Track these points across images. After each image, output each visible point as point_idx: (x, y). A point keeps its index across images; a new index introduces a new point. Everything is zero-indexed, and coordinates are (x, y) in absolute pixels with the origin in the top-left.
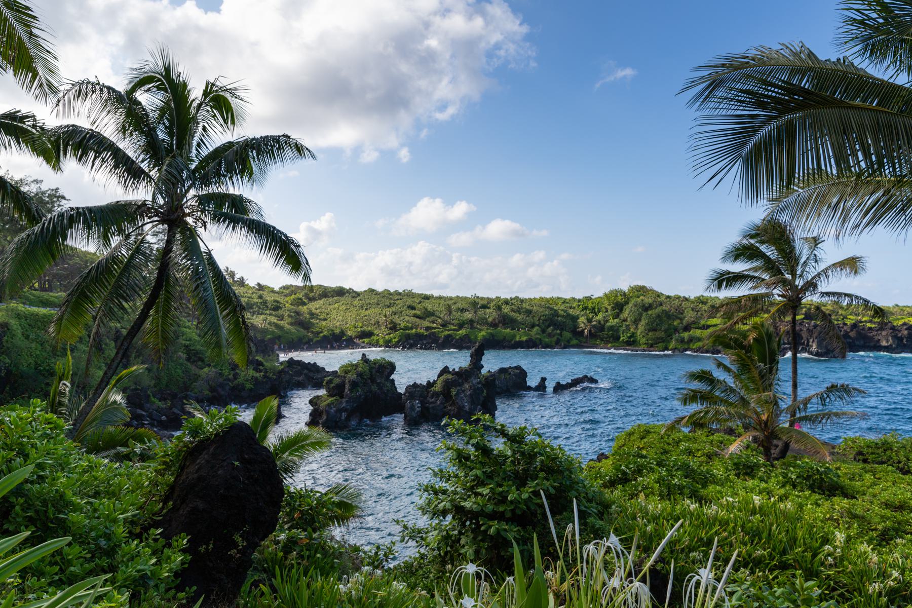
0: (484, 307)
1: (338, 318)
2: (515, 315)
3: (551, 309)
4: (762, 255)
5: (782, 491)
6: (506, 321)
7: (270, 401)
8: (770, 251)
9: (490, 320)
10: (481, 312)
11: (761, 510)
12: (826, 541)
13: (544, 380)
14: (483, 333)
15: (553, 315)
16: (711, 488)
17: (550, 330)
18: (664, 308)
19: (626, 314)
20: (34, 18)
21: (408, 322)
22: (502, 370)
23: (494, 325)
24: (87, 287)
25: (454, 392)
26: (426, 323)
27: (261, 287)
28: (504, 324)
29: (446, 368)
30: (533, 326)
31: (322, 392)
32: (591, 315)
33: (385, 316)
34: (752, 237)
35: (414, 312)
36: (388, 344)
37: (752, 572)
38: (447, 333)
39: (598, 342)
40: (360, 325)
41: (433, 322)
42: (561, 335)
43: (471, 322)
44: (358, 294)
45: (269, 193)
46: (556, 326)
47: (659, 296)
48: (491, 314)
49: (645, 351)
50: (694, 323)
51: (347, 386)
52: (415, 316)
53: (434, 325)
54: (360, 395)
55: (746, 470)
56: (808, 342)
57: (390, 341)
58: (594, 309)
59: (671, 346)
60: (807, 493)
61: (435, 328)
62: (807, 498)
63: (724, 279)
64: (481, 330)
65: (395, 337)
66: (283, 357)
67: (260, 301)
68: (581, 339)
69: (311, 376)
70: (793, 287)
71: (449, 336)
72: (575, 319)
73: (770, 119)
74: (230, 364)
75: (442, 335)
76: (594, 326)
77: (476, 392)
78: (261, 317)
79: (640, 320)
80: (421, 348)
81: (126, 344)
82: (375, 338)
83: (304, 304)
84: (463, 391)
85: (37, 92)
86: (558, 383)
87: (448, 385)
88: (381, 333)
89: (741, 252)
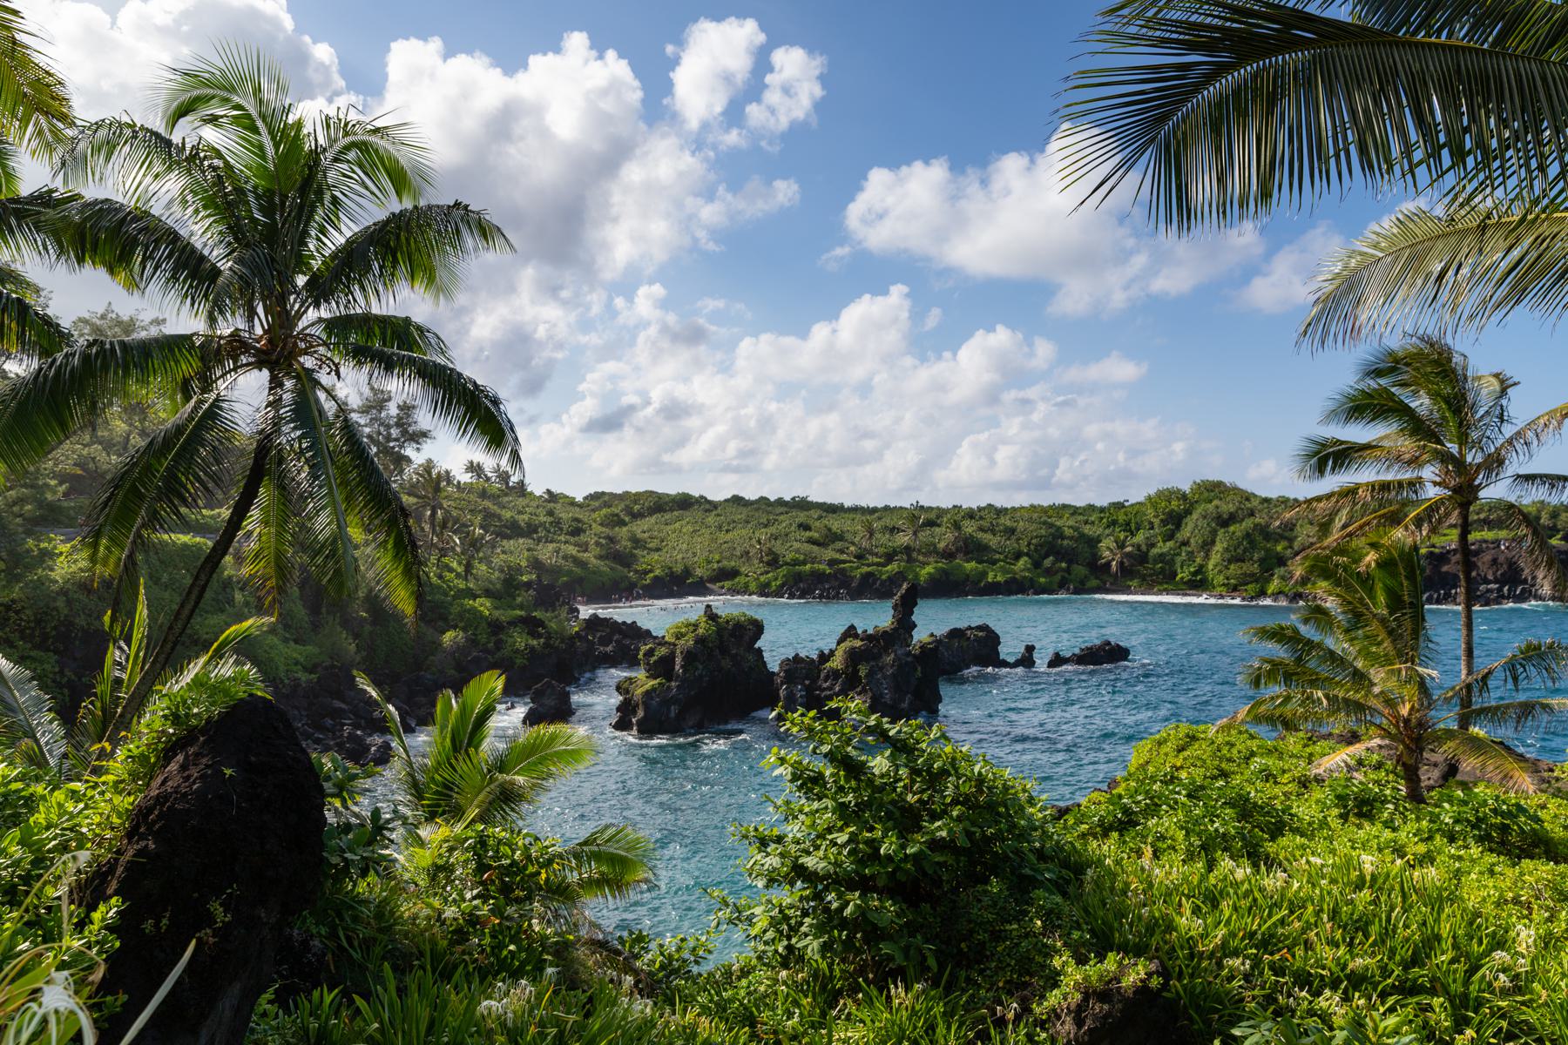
0: (931, 524)
1: (682, 545)
2: (986, 537)
3: (1051, 525)
4: (1404, 412)
5: (1422, 848)
6: (971, 548)
7: (489, 679)
8: (1421, 403)
9: (942, 545)
10: (924, 535)
11: (1375, 882)
12: (1499, 943)
14: (929, 569)
15: (1055, 537)
16: (1283, 841)
17: (1048, 562)
18: (1257, 520)
19: (1185, 532)
20: (15, 13)
21: (797, 551)
22: (955, 633)
23: (948, 555)
24: (140, 479)
25: (863, 671)
26: (829, 554)
27: (552, 497)
28: (966, 553)
29: (852, 627)
30: (1018, 556)
31: (640, 674)
32: (1122, 535)
33: (759, 542)
34: (1378, 373)
35: (808, 534)
36: (764, 591)
37: (1346, 998)
38: (865, 569)
39: (1134, 583)
40: (717, 557)
41: (842, 551)
42: (1068, 570)
43: (908, 549)
44: (714, 506)
45: (476, 313)
46: (1064, 552)
47: (1248, 499)
48: (944, 537)
49: (1222, 597)
51: (678, 660)
52: (812, 541)
53: (844, 557)
54: (701, 676)
55: (1363, 807)
56: (1534, 578)
57: (768, 585)
58: (1128, 524)
59: (1272, 587)
60: (1475, 851)
61: (844, 562)
62: (1473, 861)
63: (1328, 456)
64: (925, 564)
65: (777, 577)
66: (586, 612)
67: (550, 519)
68: (1105, 577)
69: (625, 644)
70: (1459, 463)
71: (870, 574)
72: (1093, 542)
73: (1219, 71)
74: (489, 624)
75: (857, 574)
76: (1129, 555)
77: (904, 668)
78: (551, 546)
79: (1213, 542)
80: (821, 597)
81: (203, 577)
82: (741, 580)
83: (623, 523)
84: (881, 669)
85: (34, 144)
87: (854, 657)
88: (752, 571)
89: (1361, 407)
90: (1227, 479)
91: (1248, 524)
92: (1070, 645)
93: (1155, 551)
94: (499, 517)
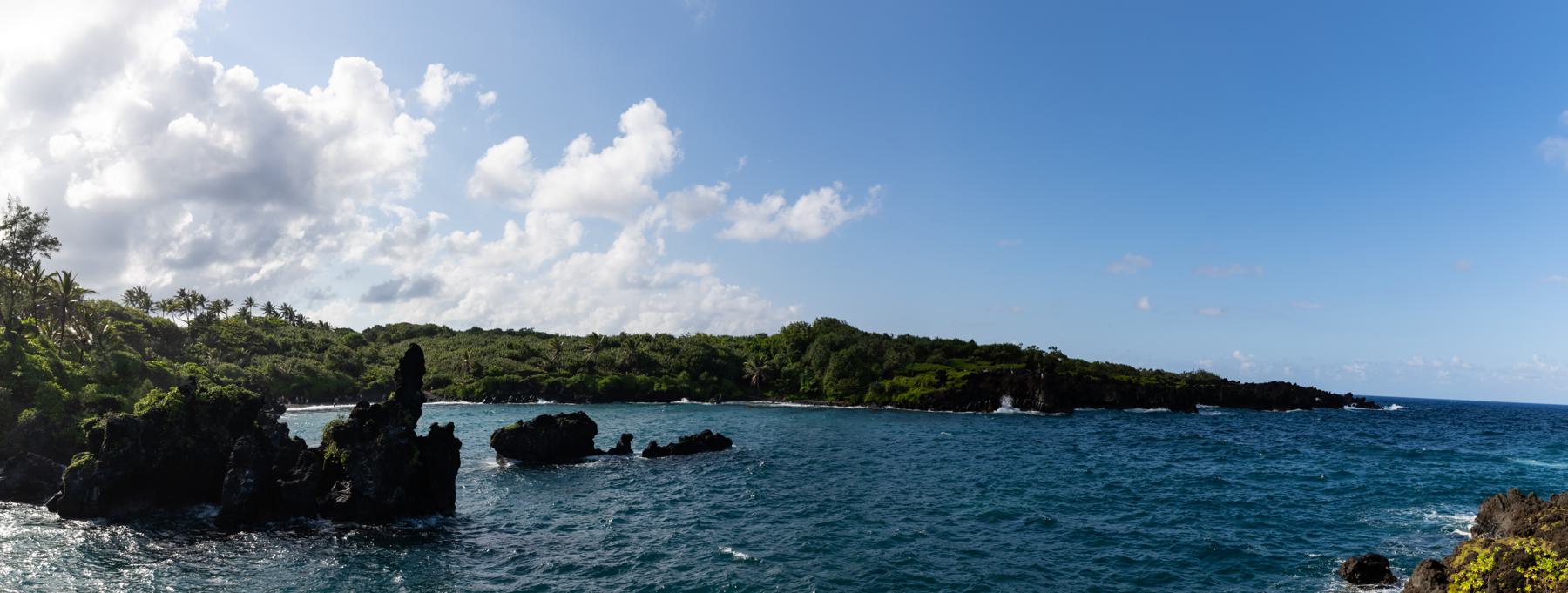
9: (619, 362)
10: (605, 353)
13: (627, 438)
14: (606, 380)
17: (703, 376)
19: (808, 356)
23: (623, 368)
26: (525, 367)
38: (552, 379)
41: (535, 365)
43: (590, 365)
44: (454, 333)
48: (621, 355)
50: (896, 367)
52: (512, 357)
57: (472, 391)
58: (768, 349)
59: (867, 398)
64: (602, 376)
65: (478, 385)
72: (740, 362)
79: (827, 363)
82: (452, 387)
86: (653, 444)
90: (840, 318)
91: (853, 348)
92: (667, 438)
93: (785, 368)
94: (261, 338)
